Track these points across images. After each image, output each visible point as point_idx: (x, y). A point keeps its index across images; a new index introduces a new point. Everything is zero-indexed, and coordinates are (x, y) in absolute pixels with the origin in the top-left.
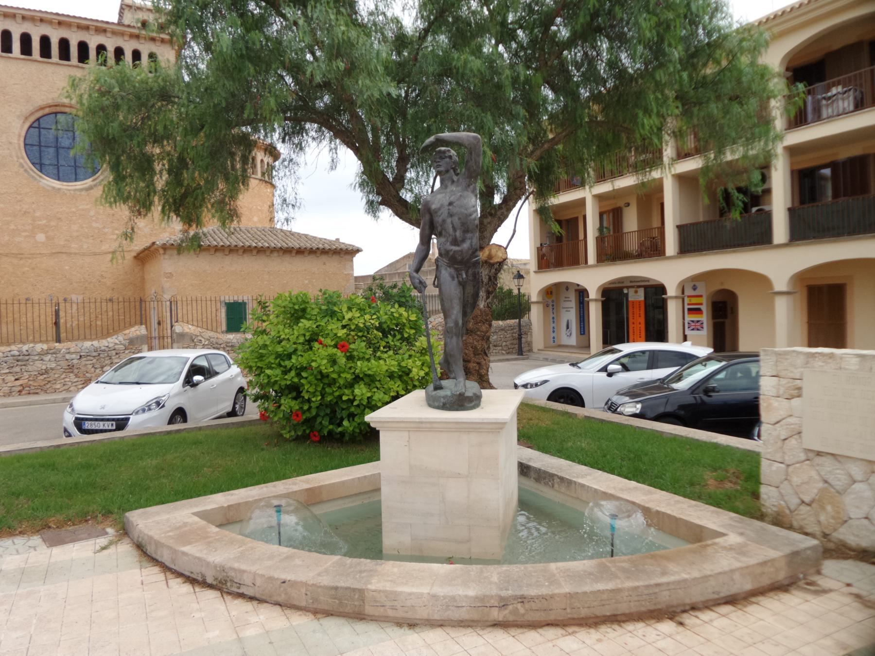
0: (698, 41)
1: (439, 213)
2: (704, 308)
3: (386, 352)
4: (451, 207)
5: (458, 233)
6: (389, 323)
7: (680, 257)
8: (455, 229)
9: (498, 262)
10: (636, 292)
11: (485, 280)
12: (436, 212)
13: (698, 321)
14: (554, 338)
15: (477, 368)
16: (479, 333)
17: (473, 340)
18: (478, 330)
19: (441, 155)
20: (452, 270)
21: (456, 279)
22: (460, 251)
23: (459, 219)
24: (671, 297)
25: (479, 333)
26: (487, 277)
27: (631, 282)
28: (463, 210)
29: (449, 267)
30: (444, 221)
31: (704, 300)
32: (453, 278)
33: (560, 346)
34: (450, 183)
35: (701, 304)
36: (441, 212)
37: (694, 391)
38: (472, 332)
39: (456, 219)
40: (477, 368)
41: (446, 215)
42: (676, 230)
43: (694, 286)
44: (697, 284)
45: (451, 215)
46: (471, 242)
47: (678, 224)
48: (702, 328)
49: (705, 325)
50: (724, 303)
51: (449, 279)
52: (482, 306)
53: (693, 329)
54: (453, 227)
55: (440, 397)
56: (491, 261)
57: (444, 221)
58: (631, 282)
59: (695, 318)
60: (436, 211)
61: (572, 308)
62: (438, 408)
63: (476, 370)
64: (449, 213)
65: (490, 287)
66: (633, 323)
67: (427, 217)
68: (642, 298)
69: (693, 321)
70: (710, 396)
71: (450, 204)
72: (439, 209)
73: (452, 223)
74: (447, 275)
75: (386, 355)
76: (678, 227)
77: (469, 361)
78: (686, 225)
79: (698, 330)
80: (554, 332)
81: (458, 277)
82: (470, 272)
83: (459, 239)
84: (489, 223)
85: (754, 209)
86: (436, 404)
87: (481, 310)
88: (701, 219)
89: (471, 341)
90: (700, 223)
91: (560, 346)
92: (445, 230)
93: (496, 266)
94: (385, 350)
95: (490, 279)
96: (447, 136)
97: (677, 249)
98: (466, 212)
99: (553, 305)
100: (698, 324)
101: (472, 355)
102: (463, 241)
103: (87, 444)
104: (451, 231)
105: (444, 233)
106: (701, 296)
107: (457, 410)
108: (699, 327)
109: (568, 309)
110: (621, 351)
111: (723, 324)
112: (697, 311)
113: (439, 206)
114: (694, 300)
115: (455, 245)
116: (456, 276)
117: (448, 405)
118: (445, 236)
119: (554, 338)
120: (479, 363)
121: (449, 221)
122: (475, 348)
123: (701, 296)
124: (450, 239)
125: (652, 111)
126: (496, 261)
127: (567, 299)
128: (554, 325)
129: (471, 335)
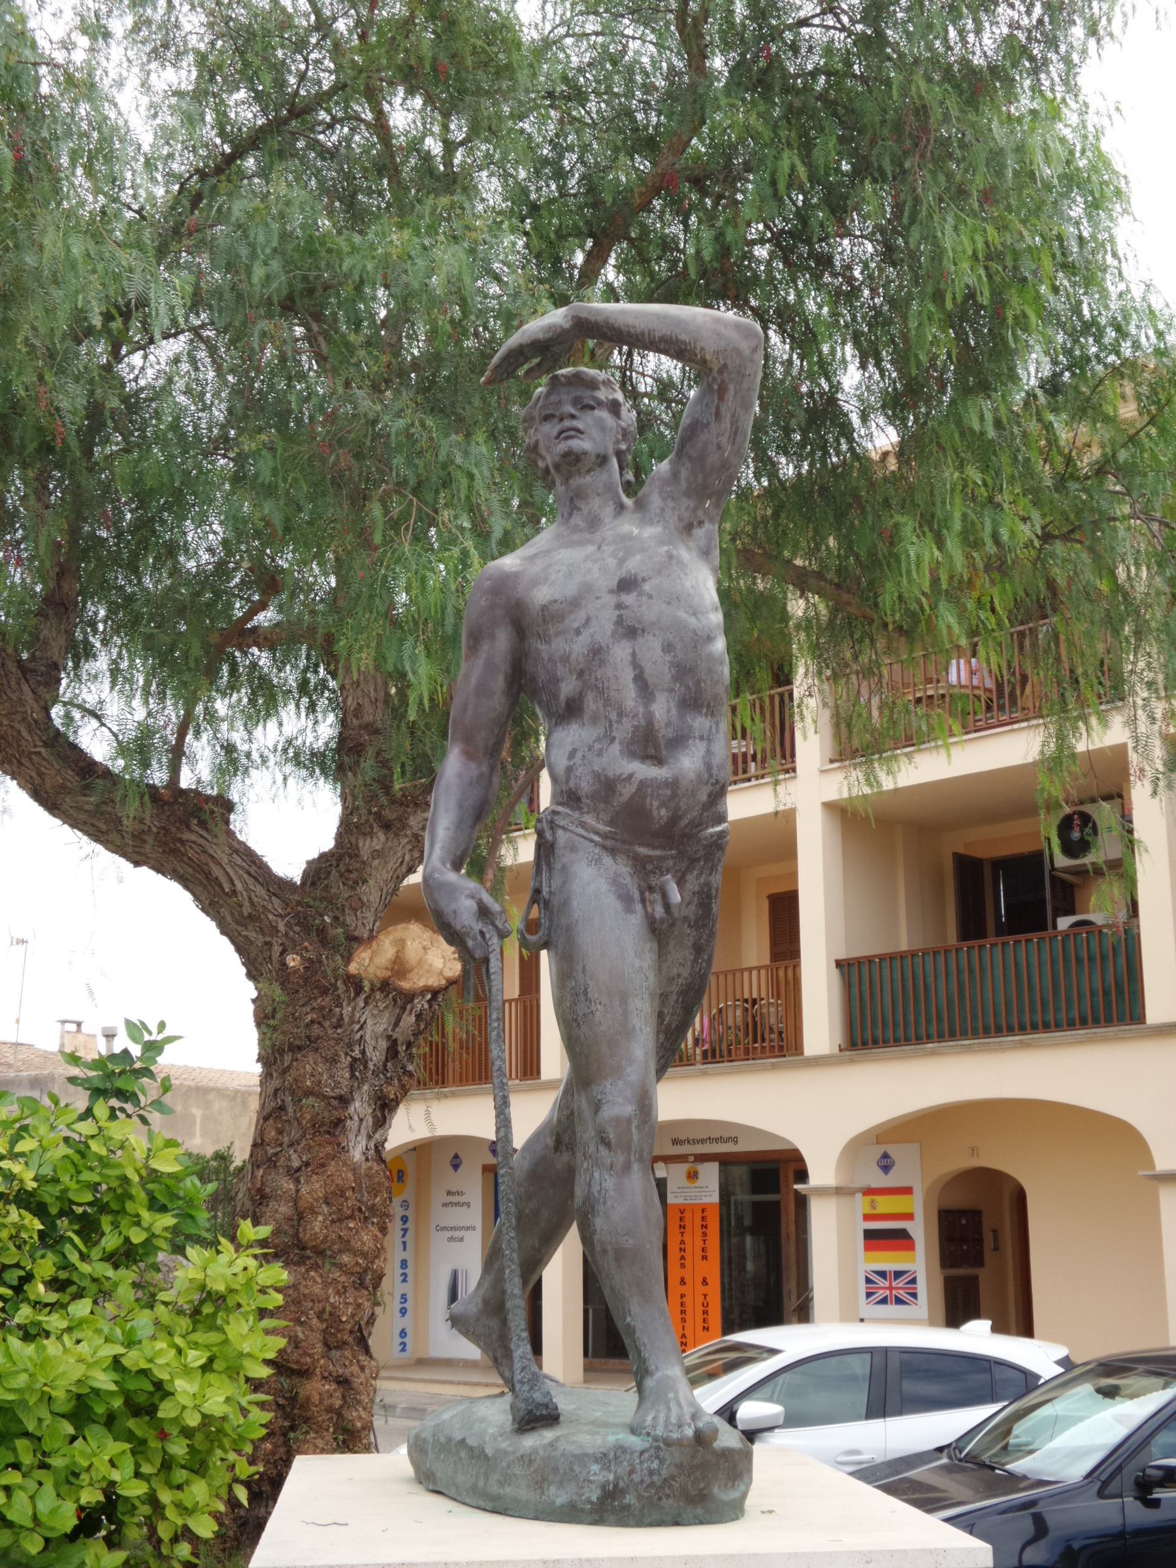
0: (904, 420)
1: (575, 620)
2: (918, 1229)
3: (52, 1307)
4: (629, 599)
5: (662, 709)
6: (65, 1179)
7: (852, 1061)
8: (644, 688)
9: (426, 990)
10: (693, 1176)
11: (376, 1056)
12: (559, 617)
13: (898, 1274)
14: (403, 1334)
15: (338, 1403)
16: (346, 1258)
17: (326, 1285)
18: (346, 1246)
19: (579, 392)
20: (622, 868)
21: (639, 907)
22: (666, 784)
23: (668, 648)
24: (823, 1191)
25: (346, 1258)
26: (383, 1044)
27: (675, 1142)
28: (682, 614)
29: (613, 852)
30: (597, 653)
31: (916, 1204)
32: (626, 899)
33: (422, 1363)
34: (609, 510)
35: (909, 1217)
36: (581, 615)
37: (1105, 1484)
38: (320, 1253)
39: (651, 649)
40: (338, 1403)
41: (609, 627)
42: (836, 973)
43: (885, 1156)
44: (894, 1151)
45: (630, 631)
46: (709, 752)
47: (842, 956)
48: (914, 1295)
49: (921, 1287)
50: (974, 1215)
51: (611, 902)
52: (357, 1155)
53: (884, 1301)
54: (641, 680)
55: (582, 1458)
56: (405, 985)
57: (597, 653)
58: (675, 1142)
59: (889, 1261)
60: (552, 615)
61: (474, 1228)
62: (570, 1514)
63: (330, 1409)
64: (620, 621)
65: (389, 1081)
66: (683, 1282)
67: (503, 640)
68: (715, 1198)
69: (882, 1274)
70: (1156, 1504)
71: (626, 585)
72: (575, 603)
73: (635, 664)
74: (604, 886)
75: (55, 1322)
76: (839, 964)
77: (305, 1373)
78: (870, 960)
79: (899, 1301)
80: (403, 1311)
81: (643, 901)
82: (692, 883)
83: (664, 732)
84: (376, 854)
85: (1064, 923)
86: (560, 1496)
87: (354, 1169)
88: (904, 946)
89: (317, 1289)
90: (902, 956)
91: (422, 1363)
92: (601, 692)
93: (421, 1004)
94: (52, 1297)
95: (392, 1051)
96: (623, 312)
97: (838, 1037)
98: (692, 622)
99: (405, 1219)
100: (900, 1283)
101: (319, 1349)
102: (679, 742)
103: (467, 1500)
104: (630, 696)
105: (591, 704)
106: (908, 1191)
107: (676, 1522)
108: (902, 1294)
109: (455, 1234)
110: (773, 1352)
111: (973, 1281)
112: (898, 1239)
113: (570, 589)
114: (885, 1204)
115: (645, 758)
116: (637, 896)
117: (630, 1499)
118: (595, 720)
119: (403, 1334)
120: (343, 1382)
121: (621, 652)
122: (331, 1319)
123: (908, 1191)
124: (623, 730)
125: (946, 522)
126: (422, 983)
127: (455, 1200)
128: (405, 1288)
129: (316, 1267)
